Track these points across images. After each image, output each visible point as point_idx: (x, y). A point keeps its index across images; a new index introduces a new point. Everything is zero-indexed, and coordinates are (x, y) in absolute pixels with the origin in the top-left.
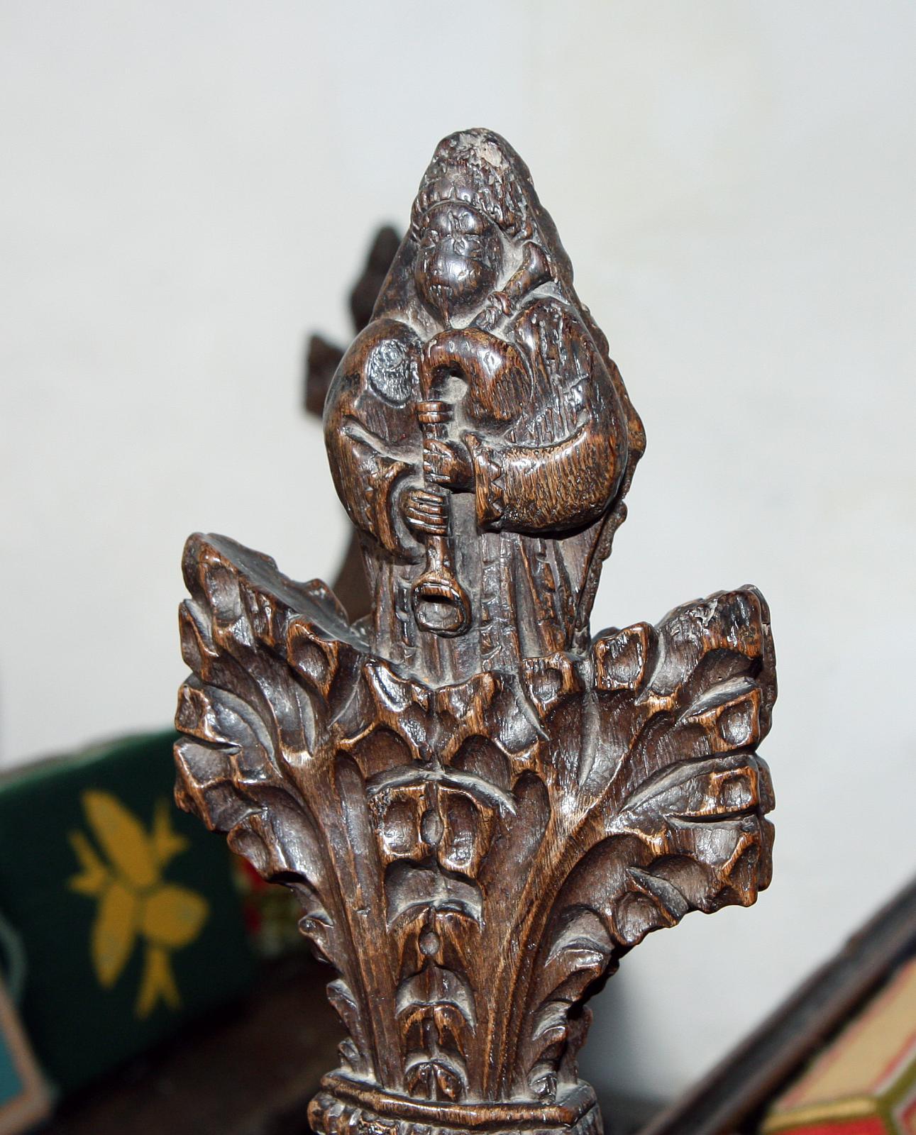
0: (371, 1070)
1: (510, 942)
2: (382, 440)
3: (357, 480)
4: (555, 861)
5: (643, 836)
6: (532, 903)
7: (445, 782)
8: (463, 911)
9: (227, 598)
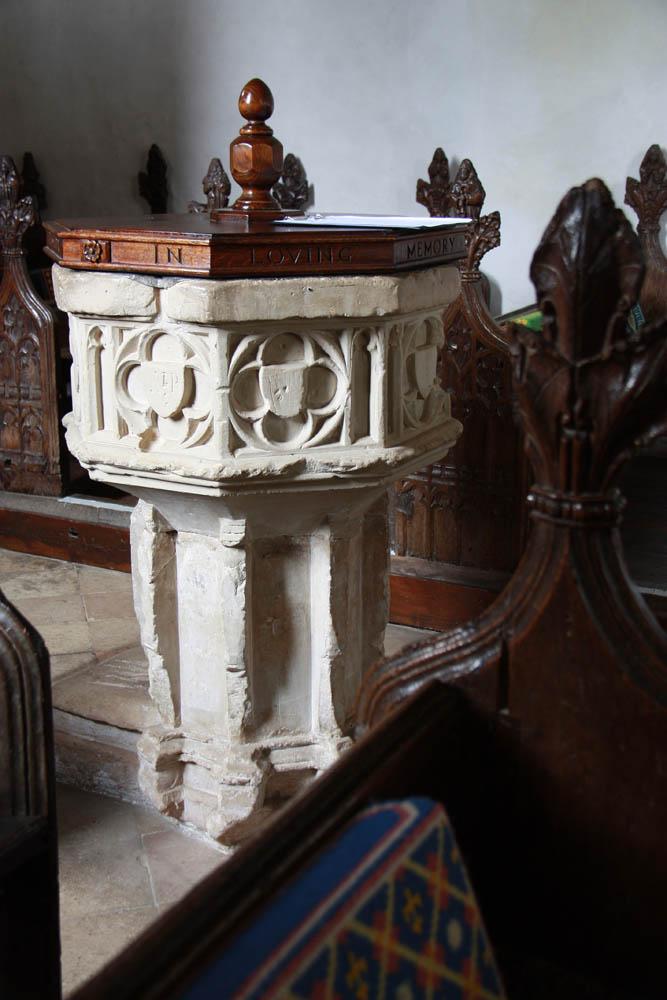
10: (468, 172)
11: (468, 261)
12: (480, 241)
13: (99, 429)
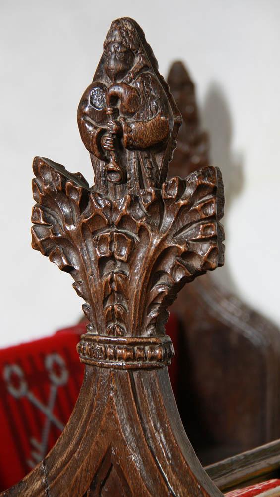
0: (96, 331)
1: (138, 283)
2: (95, 121)
3: (87, 134)
4: (152, 255)
5: (179, 246)
6: (145, 269)
7: (117, 231)
8: (123, 273)
9: (48, 176)
10: (127, 56)
11: (130, 307)
12: (163, 253)
13: (220, 487)
